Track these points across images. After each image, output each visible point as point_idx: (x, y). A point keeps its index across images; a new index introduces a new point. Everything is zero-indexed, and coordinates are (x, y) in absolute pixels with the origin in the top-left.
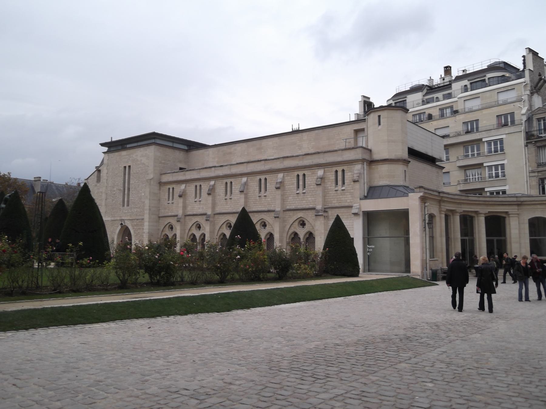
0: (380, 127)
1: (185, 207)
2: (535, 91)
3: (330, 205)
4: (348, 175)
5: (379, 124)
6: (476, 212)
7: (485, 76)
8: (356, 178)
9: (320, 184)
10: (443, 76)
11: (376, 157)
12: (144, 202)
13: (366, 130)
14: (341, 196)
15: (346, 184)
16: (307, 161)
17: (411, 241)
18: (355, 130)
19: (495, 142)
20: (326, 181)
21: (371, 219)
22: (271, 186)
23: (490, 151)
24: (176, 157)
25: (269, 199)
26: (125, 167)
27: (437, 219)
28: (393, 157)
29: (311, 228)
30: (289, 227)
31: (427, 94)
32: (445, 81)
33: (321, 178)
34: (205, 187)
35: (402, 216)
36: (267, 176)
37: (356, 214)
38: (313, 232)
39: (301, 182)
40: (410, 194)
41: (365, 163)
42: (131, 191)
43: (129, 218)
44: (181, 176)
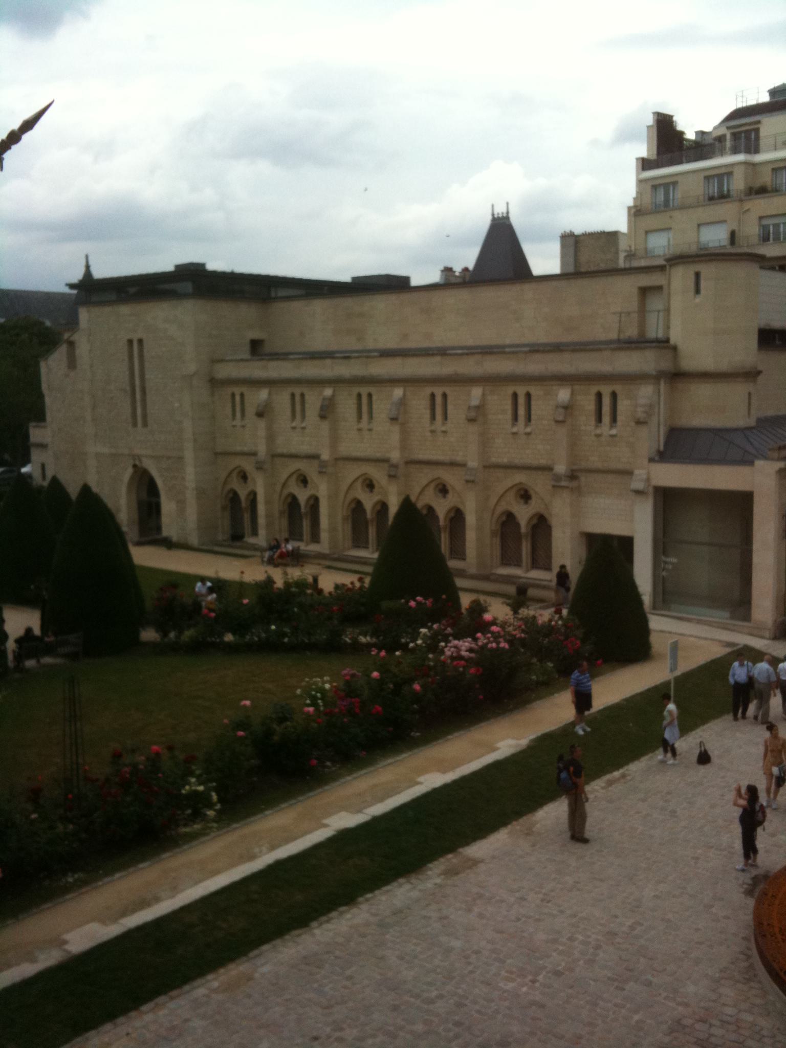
0: (698, 300)
1: (271, 438)
3: (584, 465)
4: (623, 405)
5: (697, 291)
8: (640, 415)
9: (562, 422)
11: (687, 364)
13: (665, 287)
17: (756, 559)
22: (457, 413)
24: (241, 317)
26: (130, 342)
30: (495, 501)
34: (314, 400)
35: (740, 505)
36: (448, 390)
37: (638, 492)
38: (546, 515)
39: (523, 409)
41: (662, 382)
44: (257, 370)
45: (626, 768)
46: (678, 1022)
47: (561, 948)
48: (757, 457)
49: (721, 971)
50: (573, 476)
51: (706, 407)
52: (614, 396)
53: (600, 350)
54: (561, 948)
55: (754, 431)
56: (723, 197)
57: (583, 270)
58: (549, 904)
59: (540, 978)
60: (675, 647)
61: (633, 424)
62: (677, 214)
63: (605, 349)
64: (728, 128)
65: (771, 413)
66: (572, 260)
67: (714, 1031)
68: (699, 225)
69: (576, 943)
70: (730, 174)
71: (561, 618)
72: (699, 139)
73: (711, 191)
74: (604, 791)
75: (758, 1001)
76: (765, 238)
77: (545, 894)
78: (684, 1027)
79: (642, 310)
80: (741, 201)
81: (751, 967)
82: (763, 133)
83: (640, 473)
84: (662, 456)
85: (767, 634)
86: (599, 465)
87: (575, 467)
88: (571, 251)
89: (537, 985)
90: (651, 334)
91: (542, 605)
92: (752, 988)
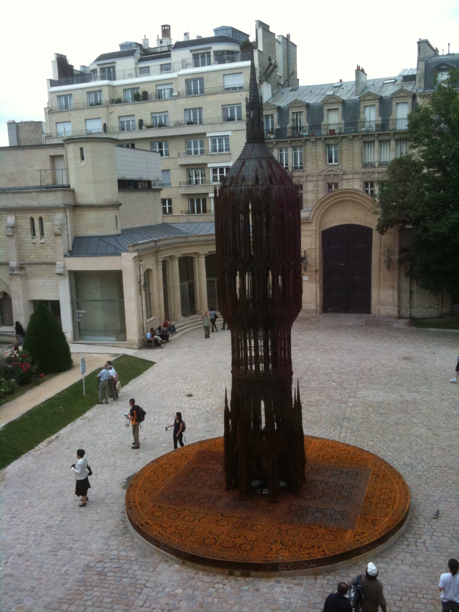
0: (83, 163)
2: (264, 78)
3: (27, 261)
4: (47, 225)
5: (83, 158)
6: (197, 254)
8: (57, 230)
10: (160, 37)
11: (82, 200)
13: (65, 157)
14: (40, 251)
17: (126, 307)
18: (51, 156)
19: (220, 138)
20: (20, 230)
23: (214, 150)
27: (154, 273)
28: (101, 202)
29: (6, 287)
31: (141, 60)
32: (163, 45)
33: (13, 227)
35: (115, 278)
37: (59, 274)
38: (8, 293)
40: (123, 254)
45: (58, 433)
46: (87, 565)
47: (21, 541)
48: (123, 252)
49: (110, 533)
50: (21, 268)
51: (94, 224)
52: (41, 219)
53: (30, 192)
54: (21, 541)
55: (120, 237)
56: (98, 104)
57: (23, 144)
58: (15, 519)
59: (10, 560)
60: (83, 360)
61: (53, 236)
62: (73, 113)
63: (33, 192)
64: (98, 65)
65: (129, 226)
66: (15, 138)
67: (107, 565)
68: (86, 120)
69: (30, 536)
70: (100, 91)
71: (18, 352)
72: (82, 70)
73: (91, 101)
74: (46, 448)
75: (130, 543)
76: (123, 129)
77: (13, 514)
78: (90, 567)
79: (53, 169)
80: (108, 107)
81: (126, 527)
82: (117, 69)
83: (60, 264)
84: (71, 253)
85: (136, 347)
86: (36, 260)
87: (22, 262)
88: (14, 132)
89: (8, 564)
90: (60, 183)
91: (8, 346)
92: (126, 537)
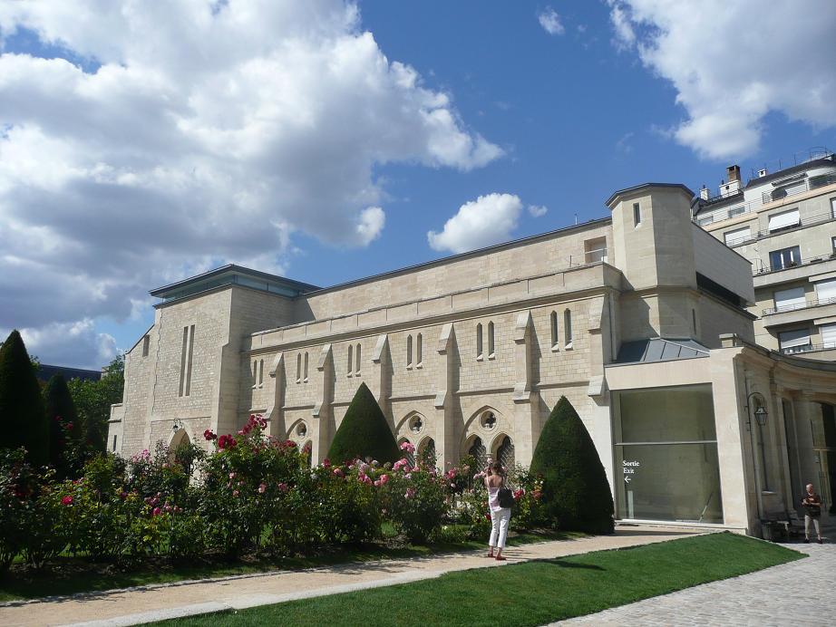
4: (576, 320)
7: (805, 175)
12: (212, 387)
15: (573, 338)
16: (497, 299)
21: (625, 406)
25: (425, 374)
34: (317, 355)
42: (193, 369)
43: (188, 415)
